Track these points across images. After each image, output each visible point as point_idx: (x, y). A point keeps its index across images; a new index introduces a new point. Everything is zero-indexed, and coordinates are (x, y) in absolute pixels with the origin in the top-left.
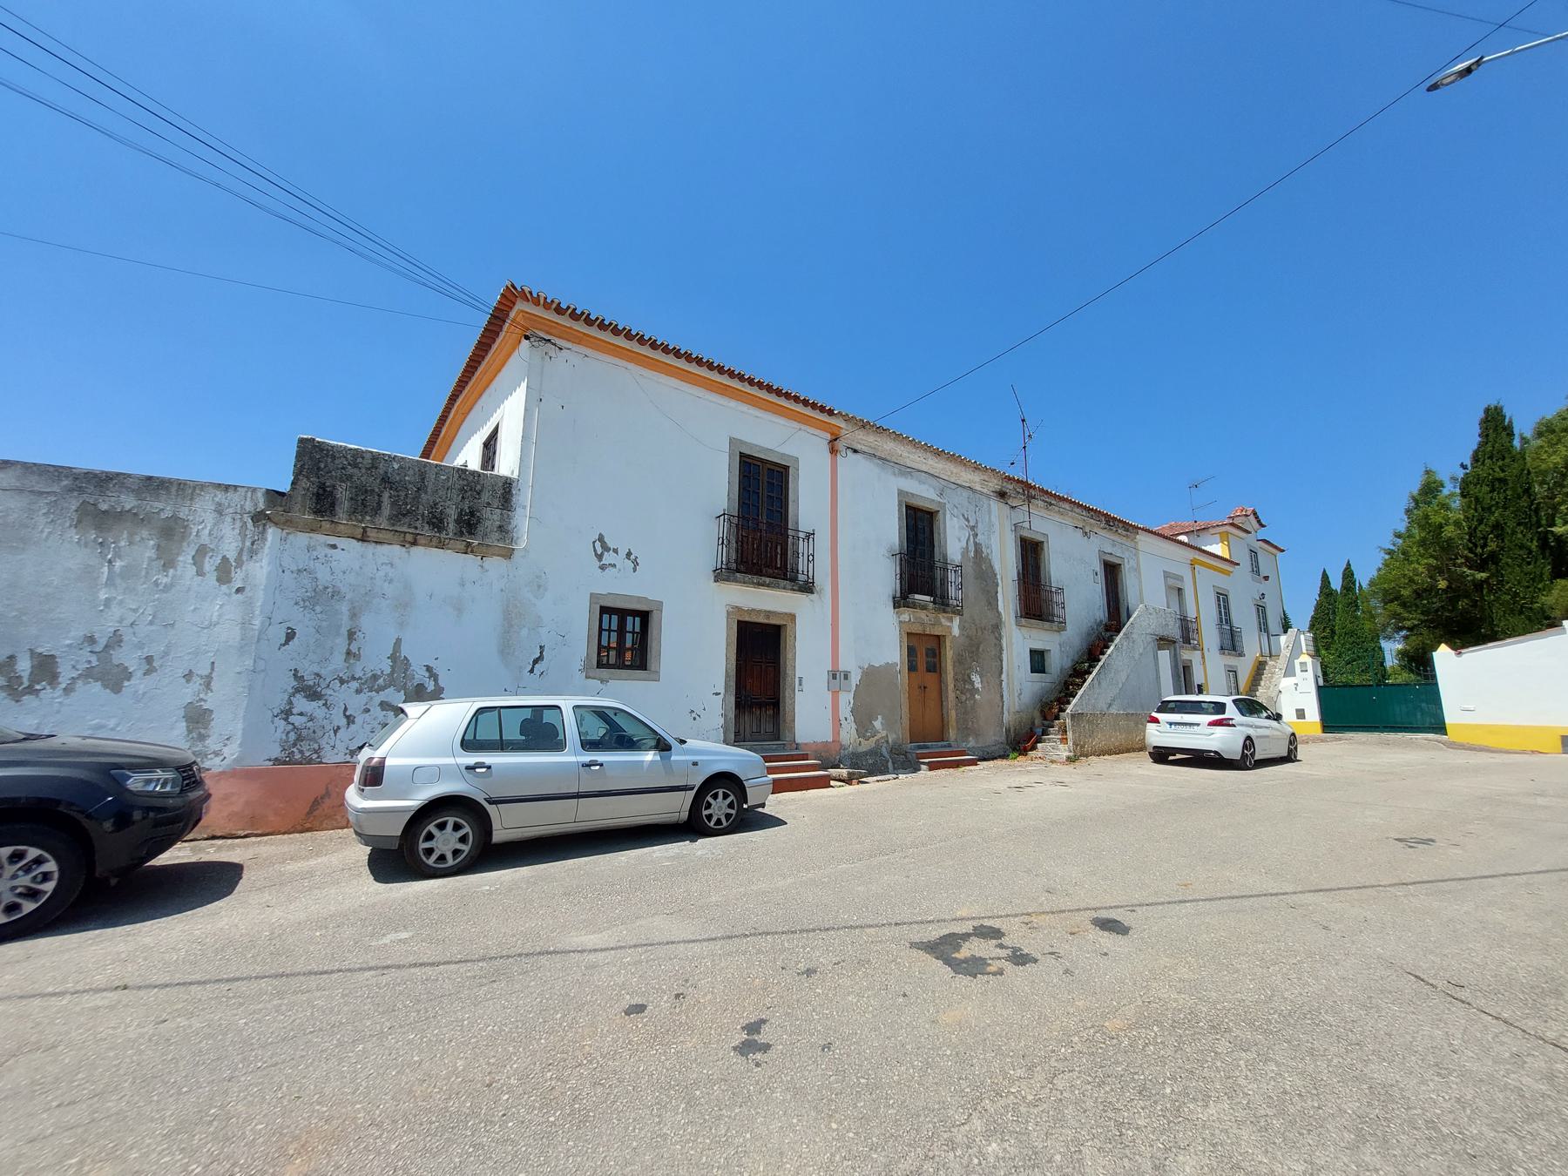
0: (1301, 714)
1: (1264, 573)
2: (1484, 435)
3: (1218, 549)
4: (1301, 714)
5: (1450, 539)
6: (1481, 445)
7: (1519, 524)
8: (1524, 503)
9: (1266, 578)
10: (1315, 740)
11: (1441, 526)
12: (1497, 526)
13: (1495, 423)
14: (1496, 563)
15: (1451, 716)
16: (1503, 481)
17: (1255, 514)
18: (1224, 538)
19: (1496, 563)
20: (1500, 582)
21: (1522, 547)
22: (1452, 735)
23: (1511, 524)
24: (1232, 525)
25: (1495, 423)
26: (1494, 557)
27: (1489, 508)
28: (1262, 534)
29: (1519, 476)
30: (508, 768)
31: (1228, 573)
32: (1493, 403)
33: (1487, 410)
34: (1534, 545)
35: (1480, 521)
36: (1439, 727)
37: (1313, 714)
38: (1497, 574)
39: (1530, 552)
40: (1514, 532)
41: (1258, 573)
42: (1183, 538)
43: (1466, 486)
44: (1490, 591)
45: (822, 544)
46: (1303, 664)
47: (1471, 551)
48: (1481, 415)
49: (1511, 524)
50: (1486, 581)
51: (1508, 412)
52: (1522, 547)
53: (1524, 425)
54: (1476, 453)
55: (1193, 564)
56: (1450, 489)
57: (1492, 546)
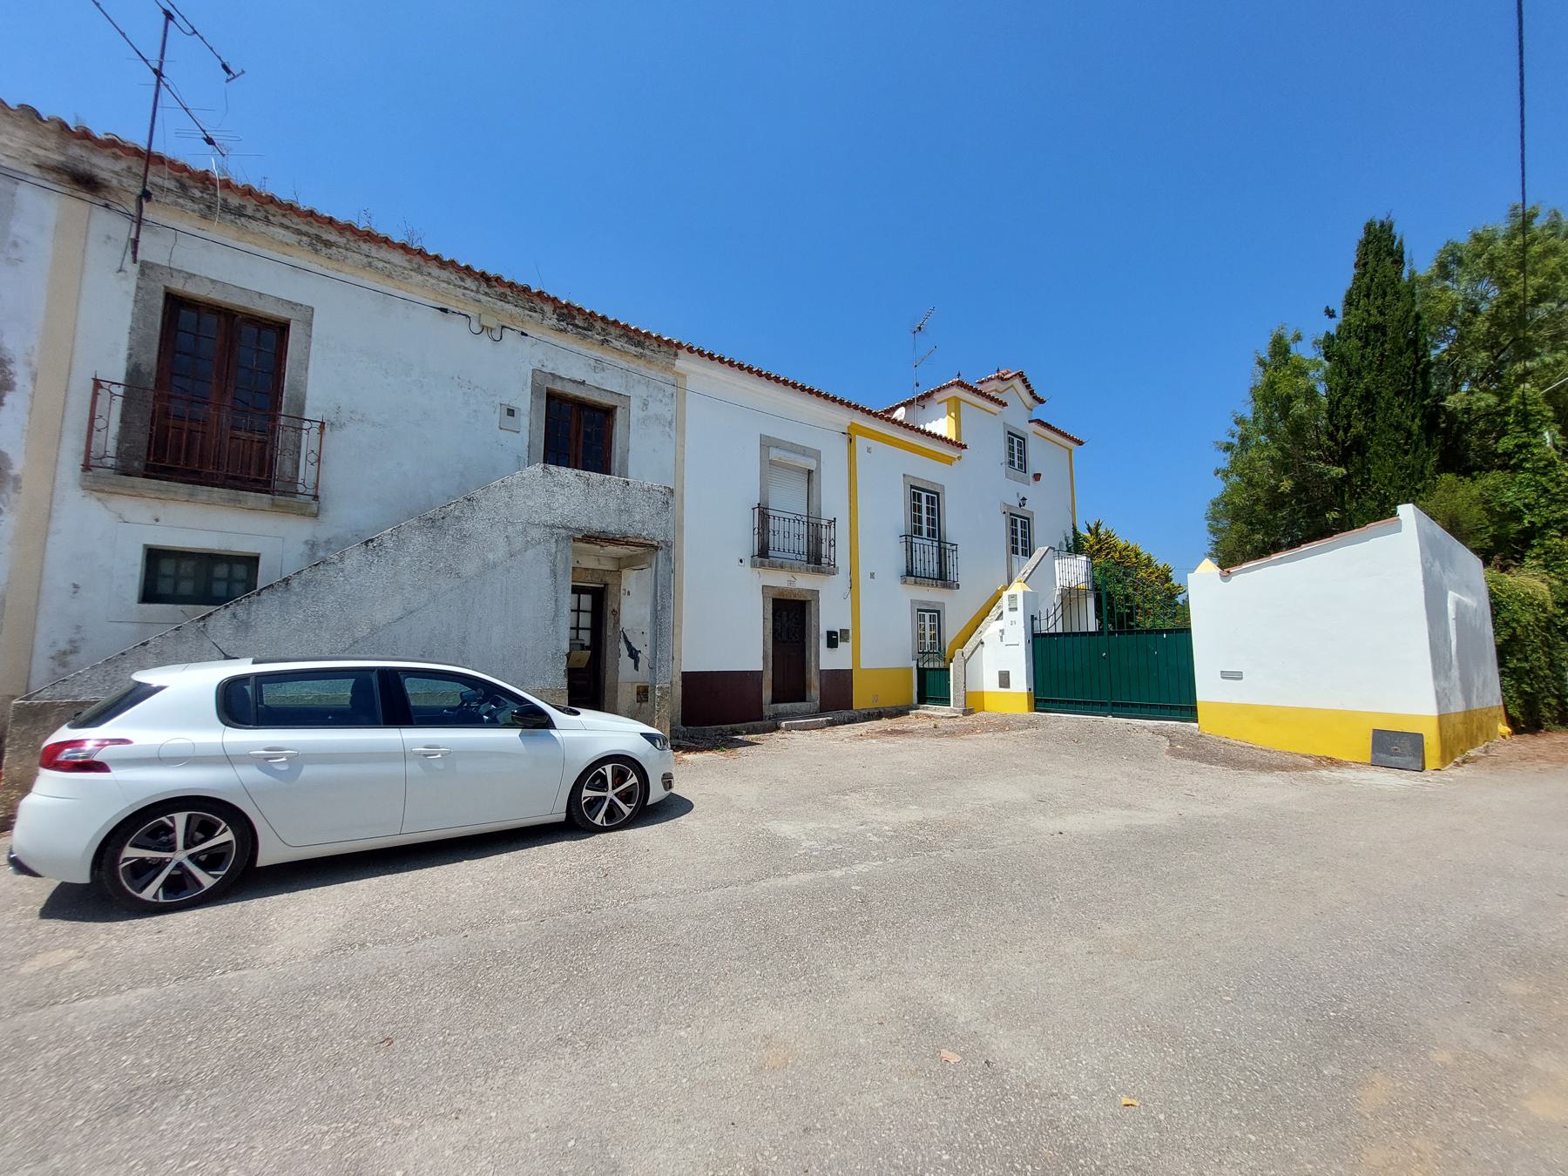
0: (1004, 679)
1: (1034, 465)
2: (1362, 265)
3: (943, 426)
4: (1004, 679)
5: (1301, 417)
6: (1356, 279)
7: (1398, 394)
9: (1037, 477)
10: (1004, 725)
11: (1289, 399)
12: (1368, 397)
13: (1380, 247)
14: (1362, 454)
15: (1208, 687)
17: (1020, 375)
18: (955, 407)
19: (1362, 454)
20: (1364, 481)
21: (1398, 427)
22: (1207, 724)
23: (1387, 393)
24: (961, 384)
25: (1380, 247)
26: (1359, 445)
27: (1358, 373)
28: (1040, 412)
29: (1403, 322)
30: (1447, 632)
31: (949, 461)
32: (1379, 217)
33: (1369, 227)
34: (1415, 426)
35: (1345, 392)
36: (1188, 710)
37: (1021, 683)
38: (1363, 469)
40: (1389, 405)
41: (1023, 467)
42: (900, 414)
43: (1329, 346)
44: (1352, 496)
45: (842, 533)
46: (1013, 597)
47: (1331, 437)
48: (1361, 235)
49: (1387, 393)
50: (1346, 480)
51: (1396, 230)
52: (1398, 427)
53: (1420, 261)
54: (1350, 294)
57: (1358, 427)
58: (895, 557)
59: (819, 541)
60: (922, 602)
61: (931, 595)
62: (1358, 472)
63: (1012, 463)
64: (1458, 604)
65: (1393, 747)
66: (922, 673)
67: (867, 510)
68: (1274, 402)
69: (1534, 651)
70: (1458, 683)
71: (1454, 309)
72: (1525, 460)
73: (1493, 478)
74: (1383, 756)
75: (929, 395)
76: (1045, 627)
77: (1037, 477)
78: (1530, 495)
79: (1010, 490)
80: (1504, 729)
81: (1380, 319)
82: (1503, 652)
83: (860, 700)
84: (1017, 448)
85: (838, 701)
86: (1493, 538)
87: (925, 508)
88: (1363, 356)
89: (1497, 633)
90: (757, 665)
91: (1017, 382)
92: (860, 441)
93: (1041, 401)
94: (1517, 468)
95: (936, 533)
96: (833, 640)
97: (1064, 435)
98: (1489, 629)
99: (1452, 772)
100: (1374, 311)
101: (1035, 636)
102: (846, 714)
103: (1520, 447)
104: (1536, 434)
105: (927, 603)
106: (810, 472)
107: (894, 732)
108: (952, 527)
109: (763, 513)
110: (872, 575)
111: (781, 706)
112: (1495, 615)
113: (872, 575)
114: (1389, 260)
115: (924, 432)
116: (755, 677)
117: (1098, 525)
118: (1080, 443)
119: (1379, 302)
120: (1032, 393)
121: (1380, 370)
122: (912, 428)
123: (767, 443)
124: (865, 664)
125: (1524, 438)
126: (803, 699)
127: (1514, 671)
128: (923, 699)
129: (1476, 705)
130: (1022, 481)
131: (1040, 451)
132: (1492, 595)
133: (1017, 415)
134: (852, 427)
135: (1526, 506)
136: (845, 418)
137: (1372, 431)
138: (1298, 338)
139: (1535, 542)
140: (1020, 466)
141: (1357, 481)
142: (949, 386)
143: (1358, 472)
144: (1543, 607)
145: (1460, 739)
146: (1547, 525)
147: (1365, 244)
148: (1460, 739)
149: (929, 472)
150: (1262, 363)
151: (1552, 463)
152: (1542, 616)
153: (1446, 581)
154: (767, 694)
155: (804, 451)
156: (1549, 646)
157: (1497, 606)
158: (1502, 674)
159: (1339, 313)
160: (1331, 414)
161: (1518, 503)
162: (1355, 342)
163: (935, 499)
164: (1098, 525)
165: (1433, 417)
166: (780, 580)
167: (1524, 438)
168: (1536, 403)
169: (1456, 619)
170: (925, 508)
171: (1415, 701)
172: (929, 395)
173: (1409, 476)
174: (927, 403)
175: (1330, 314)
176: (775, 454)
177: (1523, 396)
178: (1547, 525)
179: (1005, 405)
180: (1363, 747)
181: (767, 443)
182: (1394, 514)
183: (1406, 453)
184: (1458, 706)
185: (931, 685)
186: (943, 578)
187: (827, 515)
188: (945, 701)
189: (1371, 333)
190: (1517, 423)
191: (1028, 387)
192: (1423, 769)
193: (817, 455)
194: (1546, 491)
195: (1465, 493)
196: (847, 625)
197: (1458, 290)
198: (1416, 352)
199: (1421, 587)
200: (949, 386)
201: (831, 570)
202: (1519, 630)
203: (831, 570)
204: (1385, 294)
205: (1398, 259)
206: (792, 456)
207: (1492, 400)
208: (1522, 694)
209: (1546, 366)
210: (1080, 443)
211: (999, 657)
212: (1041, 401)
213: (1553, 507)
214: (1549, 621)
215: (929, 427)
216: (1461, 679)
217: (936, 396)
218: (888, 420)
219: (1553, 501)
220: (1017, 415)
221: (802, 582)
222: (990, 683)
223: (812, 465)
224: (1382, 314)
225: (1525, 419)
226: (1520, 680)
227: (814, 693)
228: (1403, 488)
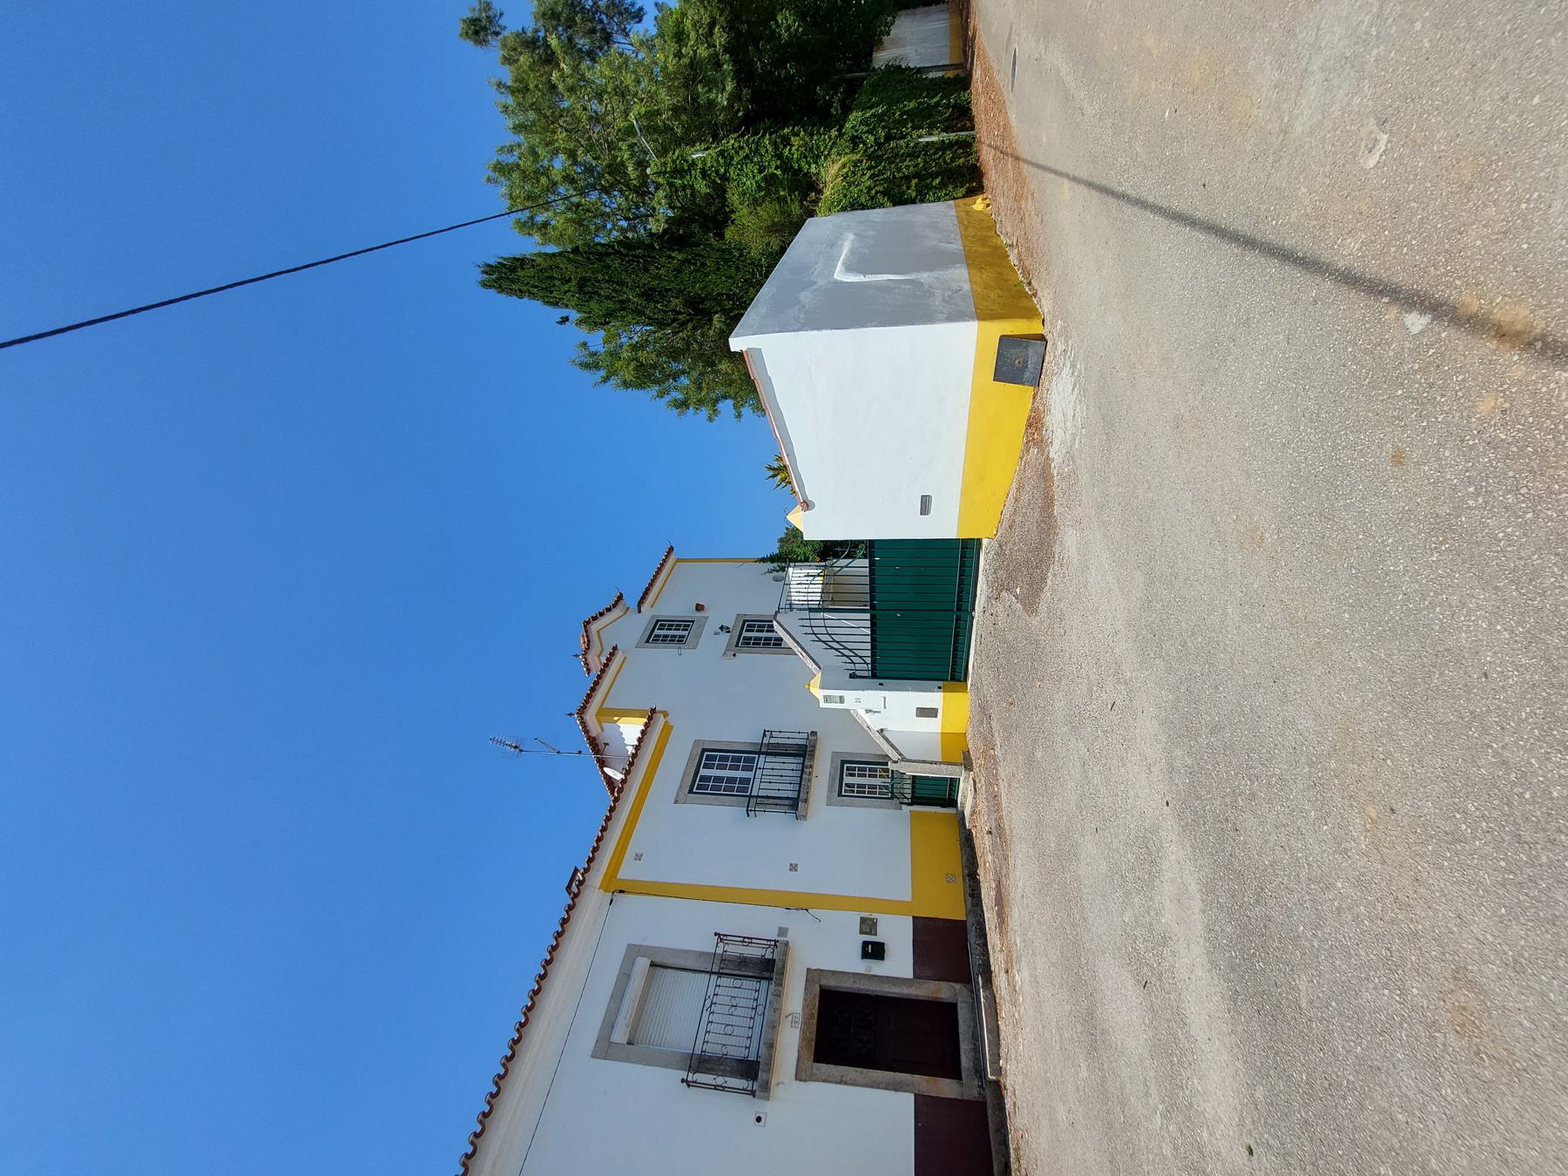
2: (520, 293)
3: (630, 730)
6: (532, 295)
7: (646, 270)
8: (616, 263)
10: (983, 712)
12: (648, 294)
13: (507, 276)
14: (702, 301)
15: (943, 526)
16: (582, 283)
17: (587, 624)
18: (608, 714)
19: (702, 301)
21: (678, 271)
22: (985, 530)
23: (645, 279)
24: (582, 710)
25: (507, 276)
28: (631, 600)
30: (879, 287)
31: (668, 729)
33: (485, 285)
35: (640, 313)
36: (964, 552)
37: (933, 698)
39: (687, 261)
40: (658, 277)
41: (686, 624)
43: (590, 322)
47: (683, 324)
48: (492, 293)
49: (645, 279)
51: (492, 262)
52: (678, 271)
53: (530, 246)
55: (618, 889)
56: (597, 339)
58: (773, 823)
59: (743, 962)
60: (830, 790)
61: (823, 768)
62: (719, 303)
63: (681, 639)
64: (849, 268)
65: (1017, 362)
66: (916, 800)
67: (712, 870)
68: (645, 376)
69: (899, 170)
70: (937, 274)
71: (573, 221)
72: (717, 172)
73: (733, 197)
74: (1027, 374)
75: (593, 742)
76: (864, 668)
77: (699, 608)
78: (750, 168)
79: (711, 643)
80: (978, 204)
81: (574, 283)
82: (899, 200)
83: (953, 909)
84: (670, 632)
85: (953, 946)
86: (791, 191)
87: (721, 774)
88: (608, 297)
89: (882, 206)
90: (909, 1099)
91: (594, 627)
92: (629, 871)
93: (620, 598)
94: (725, 178)
95: (744, 757)
96: (874, 951)
97: (660, 570)
98: (876, 215)
99: (1045, 304)
100: (566, 288)
101: (874, 676)
102: (972, 937)
103: (704, 174)
104: (694, 163)
105: (832, 778)
106: (653, 965)
107: (1000, 901)
108: (740, 732)
109: (700, 1063)
110: (794, 868)
111: (965, 1061)
112: (863, 207)
113: (794, 868)
114: (520, 273)
115: (637, 748)
116: (925, 1107)
117: (770, 468)
118: (671, 549)
119: (557, 283)
120: (609, 610)
121: (622, 283)
122: (631, 764)
123: (605, 1049)
124: (903, 891)
125: (697, 173)
126: (951, 1008)
127: (919, 191)
128: (951, 802)
129: (956, 246)
130: (702, 626)
131: (670, 604)
132: (844, 209)
133: (626, 629)
134: (605, 887)
135: (760, 172)
136: (593, 897)
137: (680, 291)
138: (584, 345)
139: (796, 166)
140: (686, 628)
141: (728, 304)
142: (583, 723)
143: (719, 303)
144: (856, 164)
145: (1002, 289)
146: (780, 156)
147: (501, 289)
148: (1002, 289)
149: (676, 765)
150: (606, 380)
151: (721, 153)
152: (865, 164)
153: (821, 282)
154: (946, 1088)
155: (625, 976)
156: (895, 157)
157: (855, 206)
158: (922, 201)
159: (564, 312)
160: (662, 325)
161: (758, 177)
162: (593, 304)
163: (708, 755)
164: (770, 468)
165: (674, 238)
166: (790, 1041)
167: (697, 173)
168: (665, 164)
169: (865, 273)
170: (721, 774)
171: (965, 344)
172: (593, 742)
173: (726, 261)
174: (601, 742)
175: (565, 320)
176: (620, 1036)
177: (658, 174)
178: (780, 156)
179: (615, 648)
180: (1019, 395)
181: (605, 1049)
182: (741, 354)
183: (703, 264)
184: (959, 276)
185: (935, 794)
186: (803, 752)
187: (708, 945)
188: (953, 783)
189: (586, 290)
190: (682, 177)
191: (601, 614)
192: (1042, 338)
193: (633, 951)
194: (747, 156)
195: (748, 225)
196: (853, 919)
197: (557, 217)
198: (608, 254)
199: (825, 332)
200: (583, 723)
201: (780, 945)
202: (880, 188)
203: (780, 945)
204: (552, 278)
205: (521, 262)
206: (621, 1018)
207: (661, 193)
208: (943, 185)
209: (632, 156)
210: (671, 549)
211: (903, 718)
212: (620, 598)
213: (763, 151)
214: (870, 158)
215: (631, 750)
216: (930, 268)
217: (594, 734)
218: (621, 791)
219: (756, 152)
220: (626, 629)
221: (796, 999)
222: (933, 726)
223: (643, 963)
224: (569, 281)
225: (678, 172)
226: (929, 188)
227: (943, 991)
228: (737, 268)
